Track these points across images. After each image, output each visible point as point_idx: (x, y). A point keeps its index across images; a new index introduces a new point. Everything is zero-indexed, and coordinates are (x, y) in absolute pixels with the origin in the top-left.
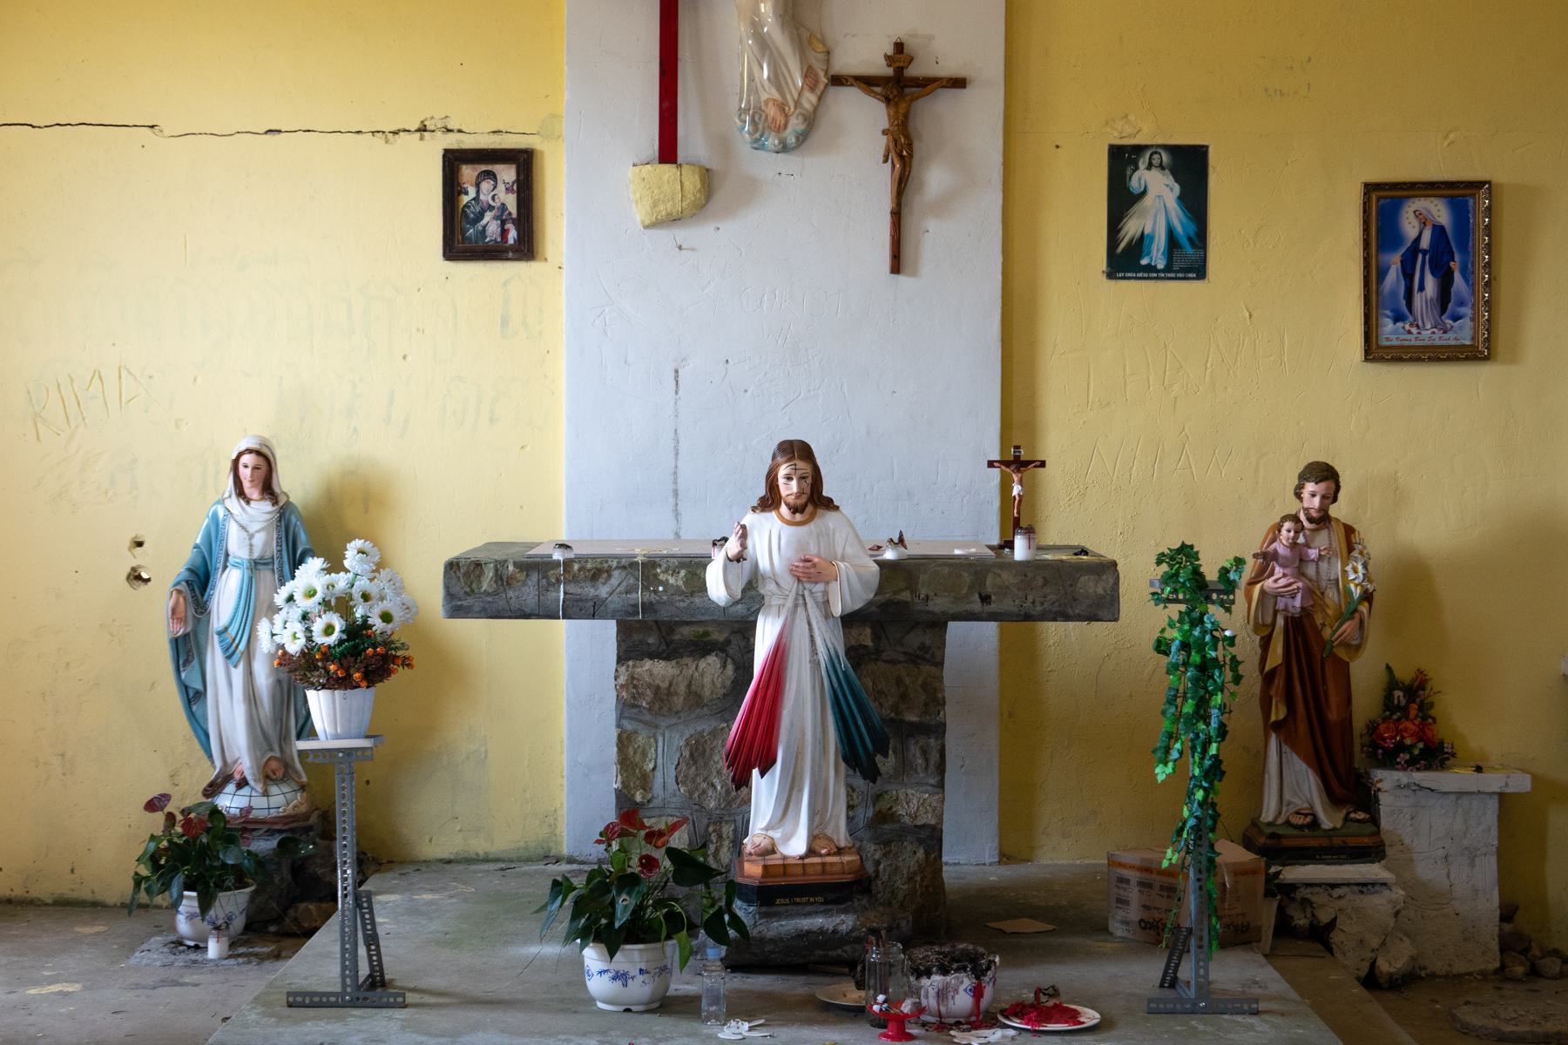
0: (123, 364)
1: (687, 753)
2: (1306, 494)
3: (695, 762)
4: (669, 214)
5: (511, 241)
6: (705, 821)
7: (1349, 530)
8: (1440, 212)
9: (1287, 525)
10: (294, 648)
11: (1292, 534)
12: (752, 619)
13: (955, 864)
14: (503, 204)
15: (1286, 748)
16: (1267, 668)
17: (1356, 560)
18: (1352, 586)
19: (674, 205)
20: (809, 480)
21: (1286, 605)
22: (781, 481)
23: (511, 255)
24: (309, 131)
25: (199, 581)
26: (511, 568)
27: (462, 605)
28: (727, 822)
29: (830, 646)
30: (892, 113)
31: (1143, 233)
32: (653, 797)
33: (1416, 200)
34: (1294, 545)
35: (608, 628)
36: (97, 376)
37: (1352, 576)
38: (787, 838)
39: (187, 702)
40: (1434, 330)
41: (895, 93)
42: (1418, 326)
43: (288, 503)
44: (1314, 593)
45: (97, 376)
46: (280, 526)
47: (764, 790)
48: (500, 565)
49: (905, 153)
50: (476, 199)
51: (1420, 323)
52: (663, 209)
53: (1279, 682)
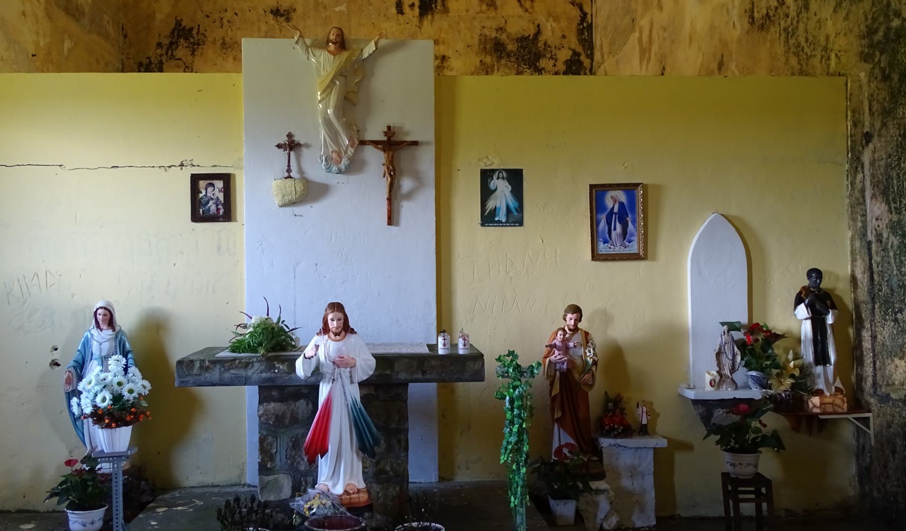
0: (48, 270)
1: (290, 445)
2: (568, 319)
3: (295, 449)
4: (290, 201)
5: (221, 213)
6: (300, 476)
7: (587, 334)
8: (622, 196)
9: (560, 332)
11: (562, 336)
12: (318, 384)
13: (419, 483)
14: (217, 197)
15: (562, 430)
16: (553, 395)
17: (590, 347)
18: (588, 359)
19: (292, 197)
20: (342, 321)
21: (560, 367)
22: (329, 322)
23: (221, 220)
24: (131, 166)
26: (207, 363)
27: (184, 381)
28: (309, 476)
29: (353, 397)
30: (386, 156)
31: (496, 207)
32: (275, 465)
33: (611, 191)
36: (36, 275)
37: (588, 354)
38: (334, 485)
39: (74, 421)
40: (621, 247)
41: (387, 147)
42: (614, 245)
43: (120, 330)
44: (571, 362)
45: (36, 275)
46: (116, 341)
47: (324, 465)
49: (392, 173)
50: (206, 195)
51: (615, 244)
53: (558, 400)
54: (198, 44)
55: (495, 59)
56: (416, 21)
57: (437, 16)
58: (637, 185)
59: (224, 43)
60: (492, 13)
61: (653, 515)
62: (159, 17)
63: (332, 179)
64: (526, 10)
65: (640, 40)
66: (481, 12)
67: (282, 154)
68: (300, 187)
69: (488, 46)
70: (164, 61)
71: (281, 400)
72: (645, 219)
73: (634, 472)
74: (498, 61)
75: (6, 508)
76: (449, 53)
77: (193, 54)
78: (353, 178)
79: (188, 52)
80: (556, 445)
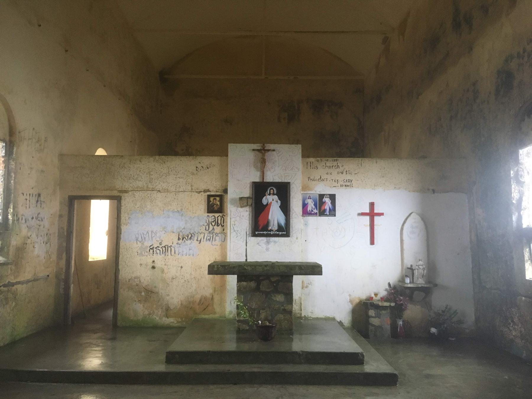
50: (213, 203)
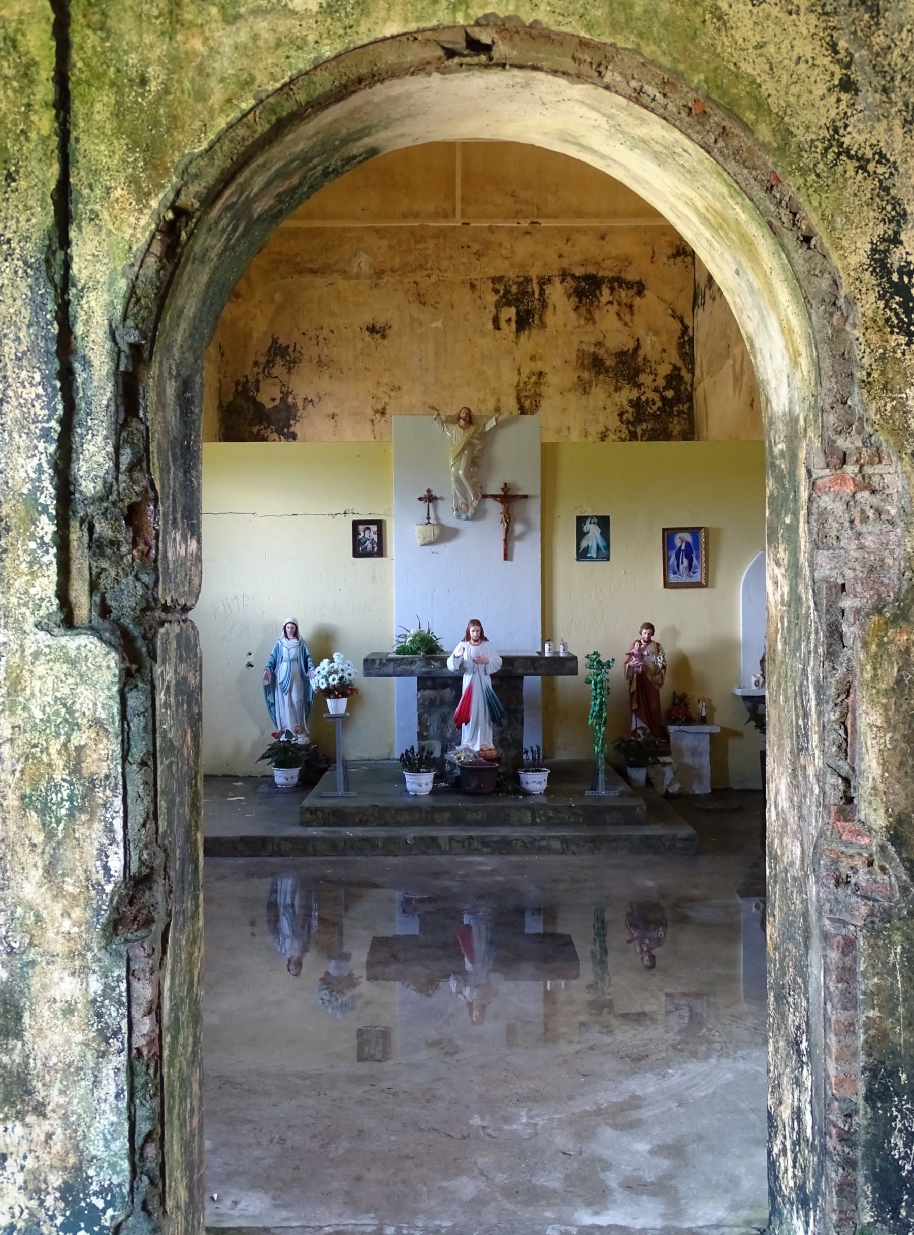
7: (658, 645)
8: (688, 537)
10: (323, 687)
25: (274, 666)
34: (640, 650)
35: (414, 680)
44: (645, 666)
48: (381, 660)
52: (427, 540)
53: (635, 696)
54: (295, 362)
55: (593, 374)
56: (512, 336)
57: (534, 331)
58: (700, 528)
59: (320, 361)
60: (590, 328)
61: (709, 785)
62: (256, 335)
63: (461, 524)
64: (626, 324)
65: (734, 366)
66: (579, 326)
67: (423, 505)
68: (437, 531)
69: (586, 362)
70: (261, 378)
71: (434, 688)
72: (707, 555)
73: (694, 752)
74: (596, 377)
75: (215, 773)
76: (546, 369)
77: (289, 372)
78: (477, 523)
79: (284, 370)
80: (634, 727)
